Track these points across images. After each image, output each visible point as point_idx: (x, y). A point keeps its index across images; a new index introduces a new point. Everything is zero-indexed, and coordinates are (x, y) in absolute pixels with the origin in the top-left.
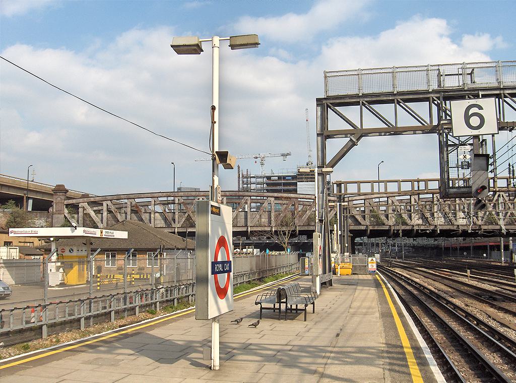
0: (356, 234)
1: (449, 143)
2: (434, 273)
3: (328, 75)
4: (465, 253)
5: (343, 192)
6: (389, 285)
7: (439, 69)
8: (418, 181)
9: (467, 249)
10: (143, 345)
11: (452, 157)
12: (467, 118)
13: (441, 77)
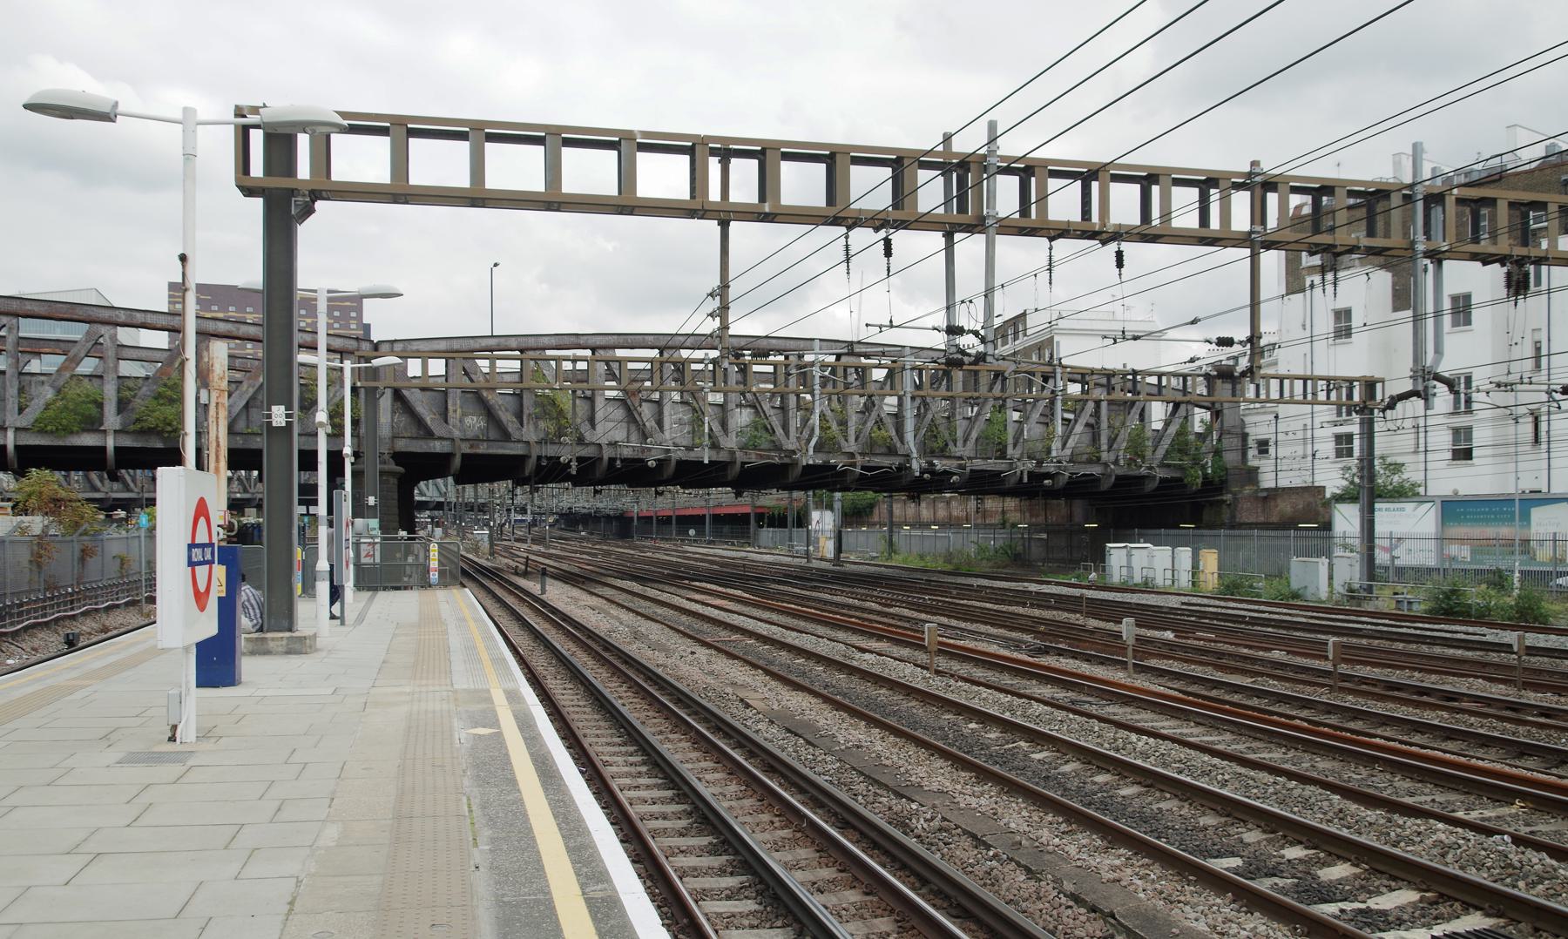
0: (417, 467)
2: (720, 589)
9: (696, 521)
10: (60, 782)
13: (1497, 272)
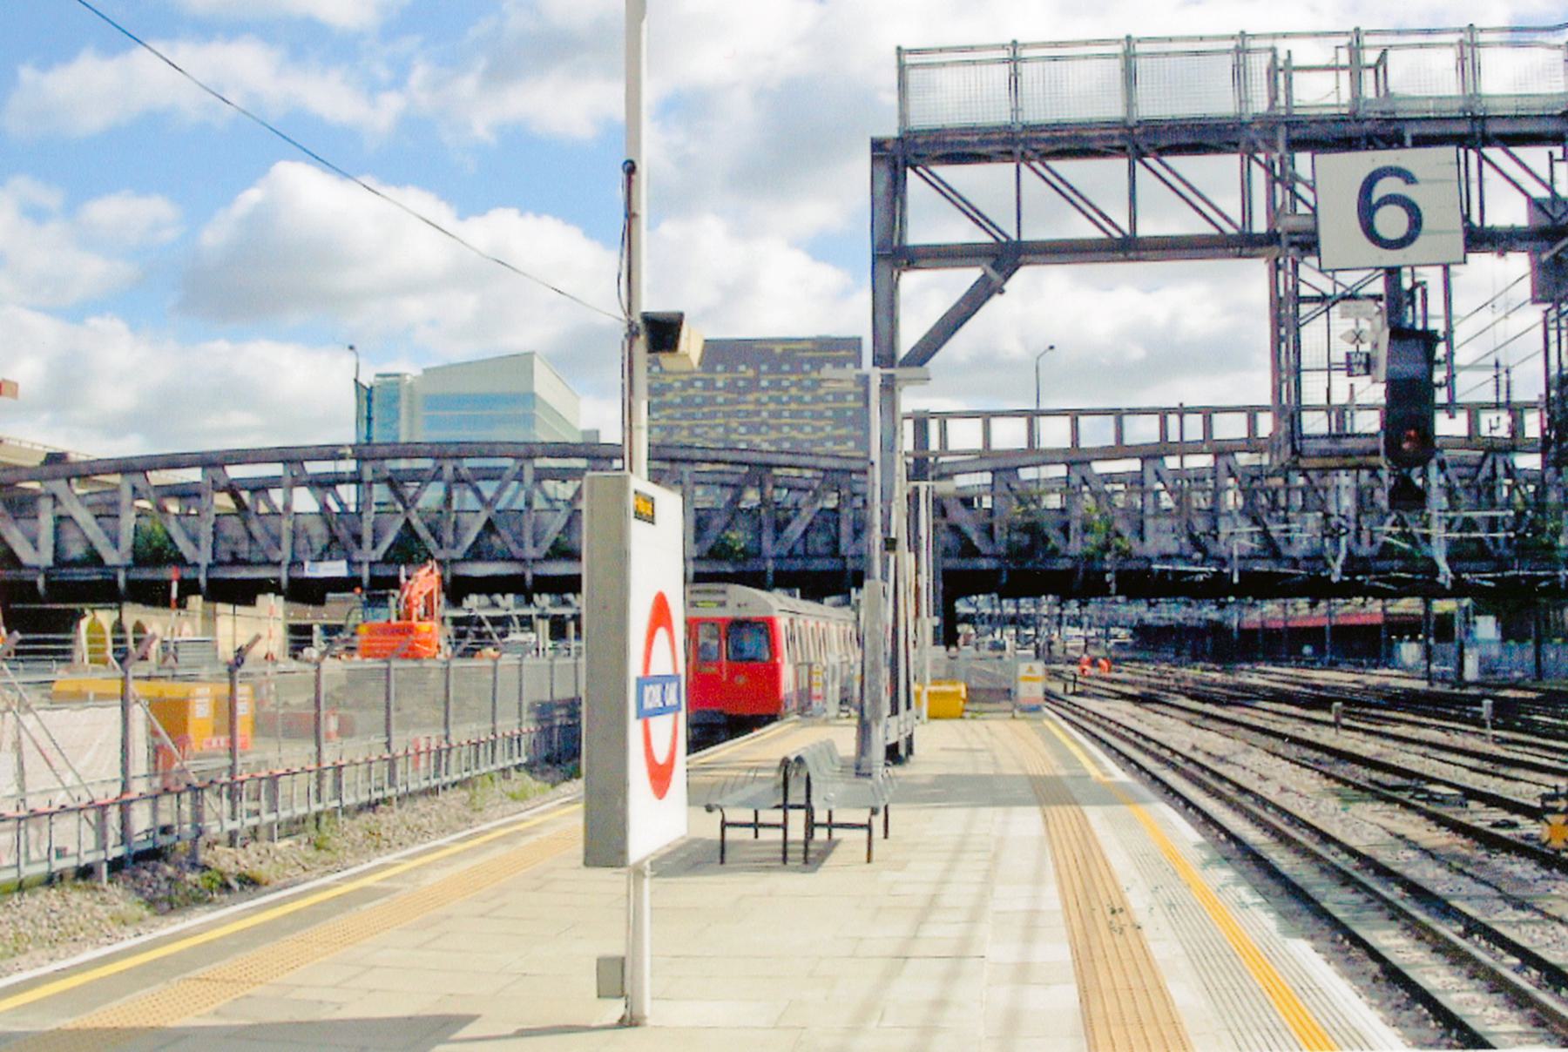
1: (1304, 291)
3: (909, 59)
4: (1307, 650)
5: (934, 444)
6: (1309, 691)
7: (1273, 50)
8: (1182, 411)
11: (1313, 337)
12: (1367, 211)
